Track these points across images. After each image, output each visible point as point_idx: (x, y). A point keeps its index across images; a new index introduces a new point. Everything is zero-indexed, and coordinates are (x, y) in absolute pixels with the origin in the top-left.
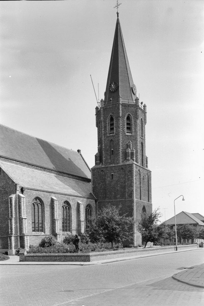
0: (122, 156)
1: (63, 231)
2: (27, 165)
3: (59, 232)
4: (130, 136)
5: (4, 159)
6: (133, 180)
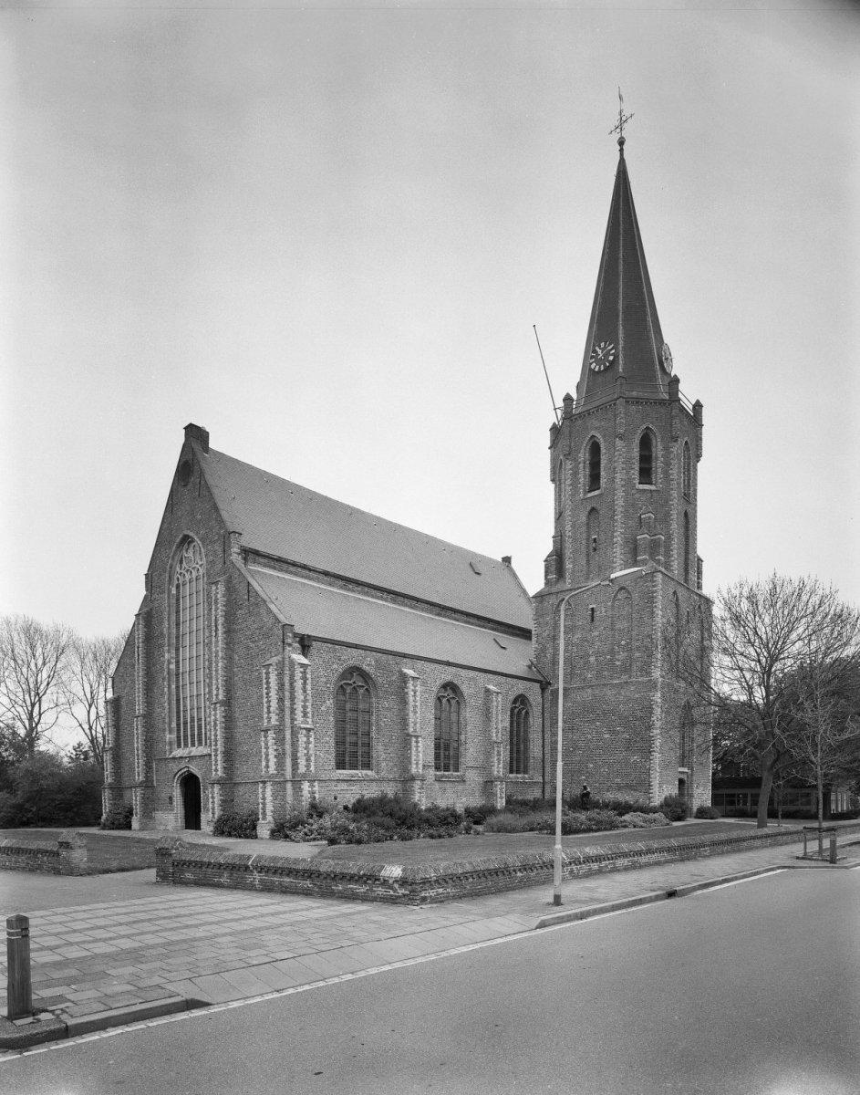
1: (437, 768)
3: (420, 771)
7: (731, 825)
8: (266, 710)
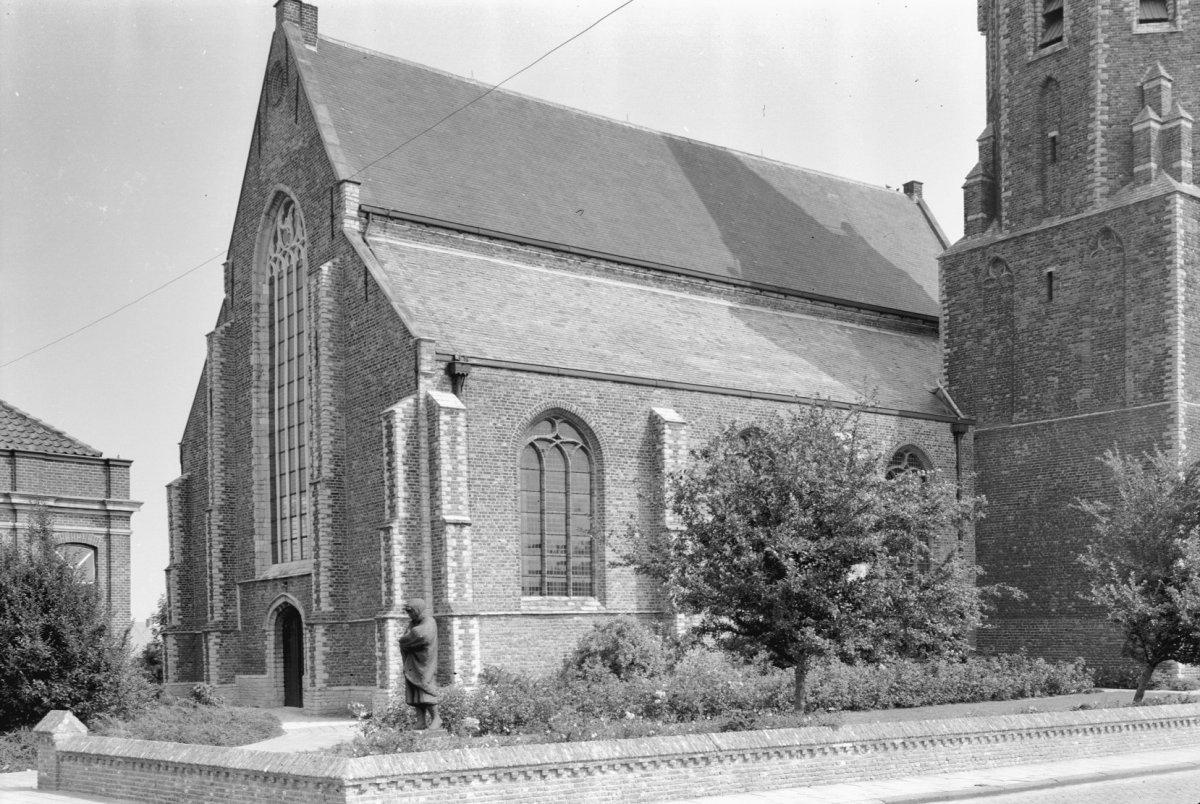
0: (1105, 159)
2: (551, 255)
4: (1163, 36)
5: (407, 226)
6: (1168, 290)
7: (994, 673)
8: (387, 492)
